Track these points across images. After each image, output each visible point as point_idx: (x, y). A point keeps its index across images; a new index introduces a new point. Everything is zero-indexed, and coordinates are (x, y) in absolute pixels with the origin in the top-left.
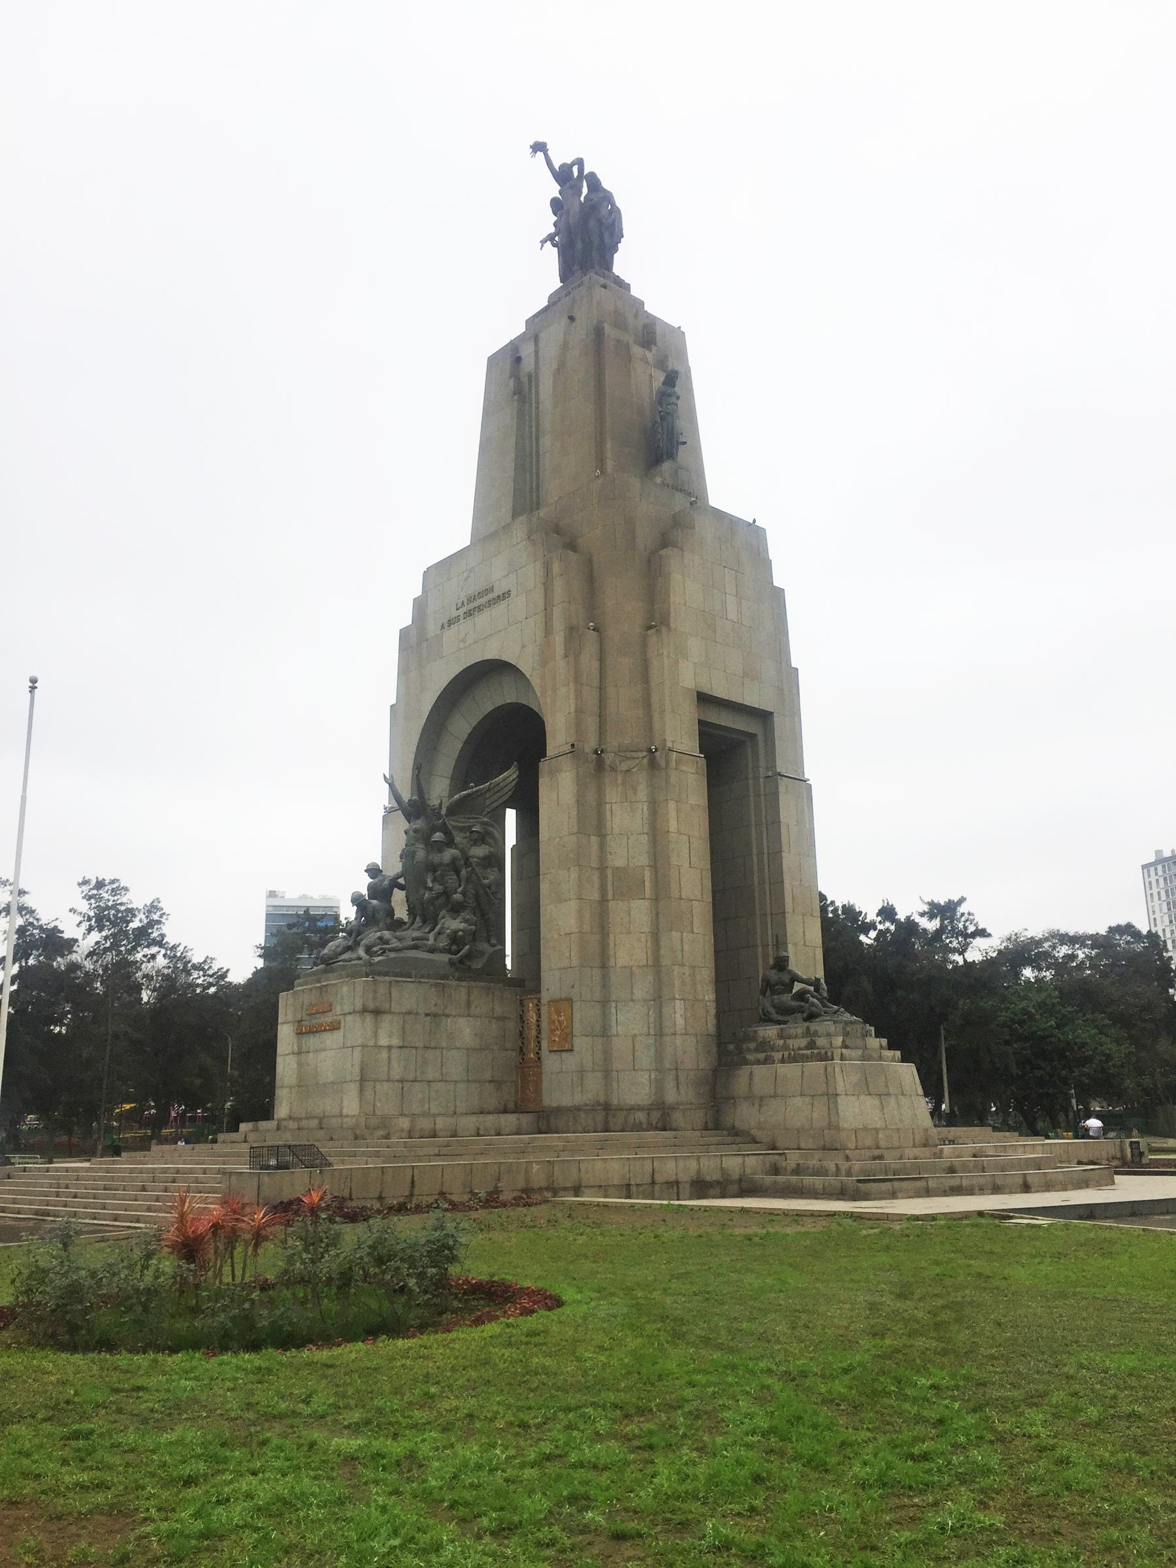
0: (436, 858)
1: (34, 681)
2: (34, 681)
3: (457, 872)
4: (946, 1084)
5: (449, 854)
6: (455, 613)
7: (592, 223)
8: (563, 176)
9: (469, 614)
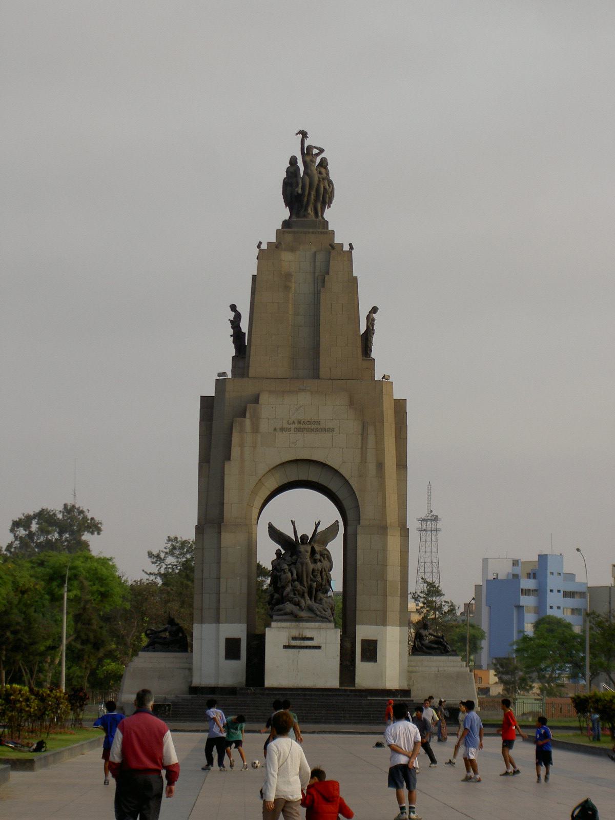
6: (286, 426)
8: (307, 152)
9: (297, 430)
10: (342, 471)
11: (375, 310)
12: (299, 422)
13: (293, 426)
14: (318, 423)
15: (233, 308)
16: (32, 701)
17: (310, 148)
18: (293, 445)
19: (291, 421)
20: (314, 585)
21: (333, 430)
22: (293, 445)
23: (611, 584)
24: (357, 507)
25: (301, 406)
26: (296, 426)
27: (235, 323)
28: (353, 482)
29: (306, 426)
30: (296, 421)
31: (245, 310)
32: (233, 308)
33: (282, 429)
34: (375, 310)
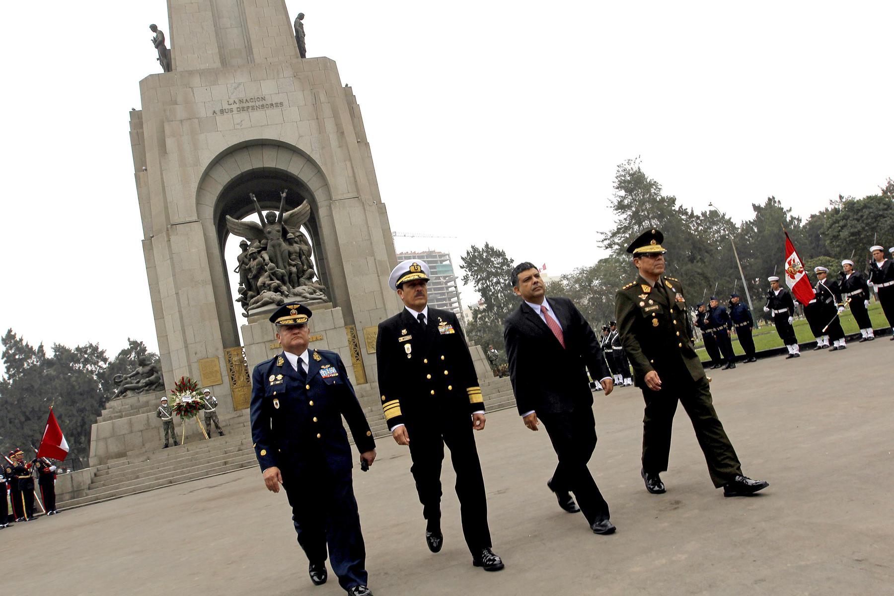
0: (291, 249)
6: (226, 106)
10: (300, 146)
11: (301, 16)
12: (241, 101)
13: (234, 107)
14: (263, 99)
15: (154, 28)
16: (617, 247)
18: (238, 127)
19: (231, 101)
20: (294, 269)
21: (281, 104)
22: (238, 127)
23: (512, 261)
24: (326, 185)
25: (240, 84)
26: (238, 106)
27: (159, 43)
28: (315, 157)
29: (245, 106)
30: (237, 101)
31: (164, 27)
32: (154, 28)
34: (301, 16)
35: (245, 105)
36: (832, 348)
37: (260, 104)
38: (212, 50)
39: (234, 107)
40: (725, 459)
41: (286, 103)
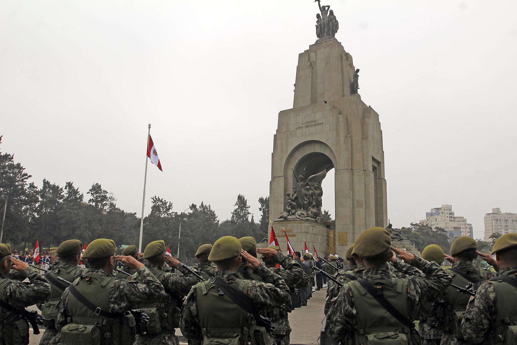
0: (307, 193)
1: (150, 125)
2: (150, 125)
3: (312, 197)
4: (5, 209)
5: (311, 192)
6: (301, 125)
7: (331, 24)
8: (323, 9)
9: (307, 127)
13: (304, 125)
17: (324, 7)
29: (308, 125)
32: (30, 176)
33: (299, 128)
35: (308, 124)
36: (384, 286)
37: (313, 124)
38: (309, 96)
39: (304, 125)
40: (438, 272)
41: (325, 123)
